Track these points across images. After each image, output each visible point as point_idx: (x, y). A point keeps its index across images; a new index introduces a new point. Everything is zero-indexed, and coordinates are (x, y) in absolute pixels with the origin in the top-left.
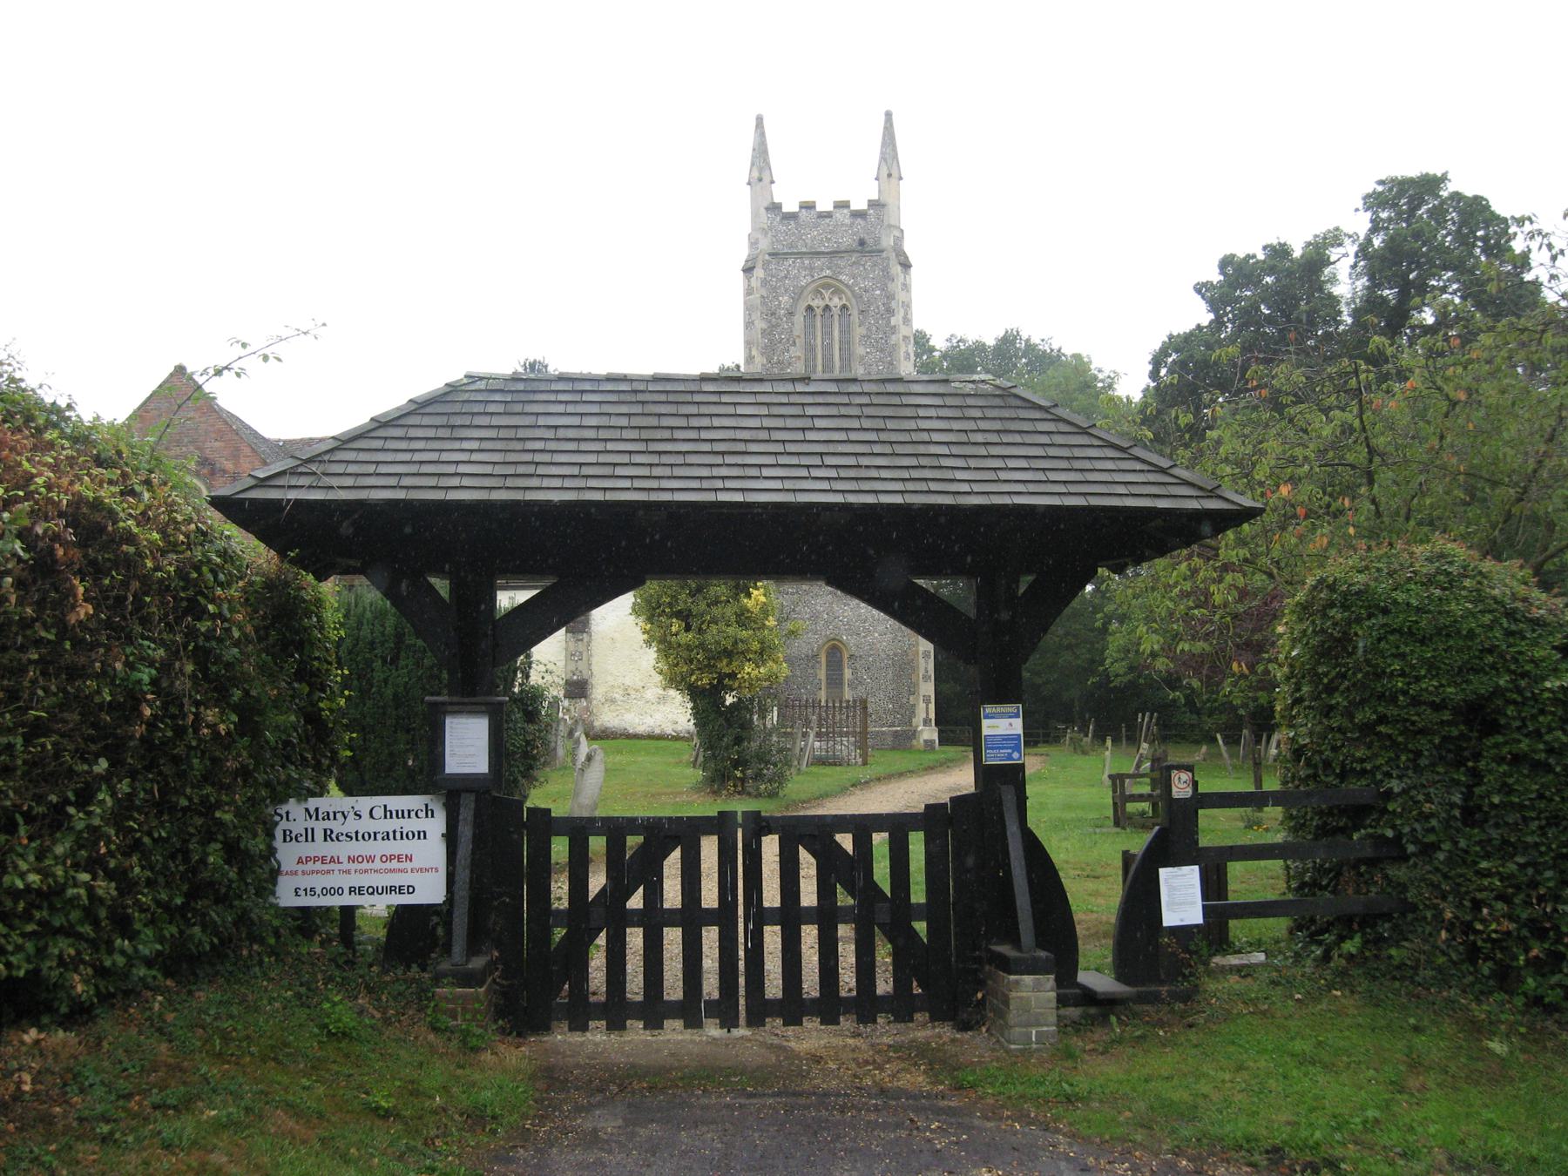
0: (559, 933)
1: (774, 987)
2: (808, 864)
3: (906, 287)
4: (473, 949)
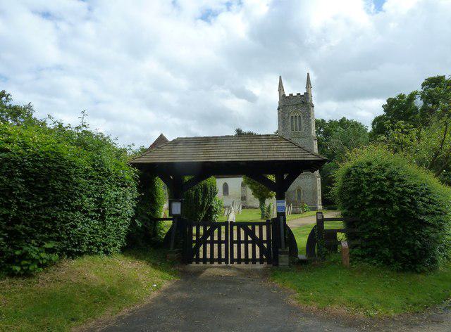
0: (194, 245)
1: (235, 256)
2: (242, 232)
3: (313, 111)
4: (175, 247)
